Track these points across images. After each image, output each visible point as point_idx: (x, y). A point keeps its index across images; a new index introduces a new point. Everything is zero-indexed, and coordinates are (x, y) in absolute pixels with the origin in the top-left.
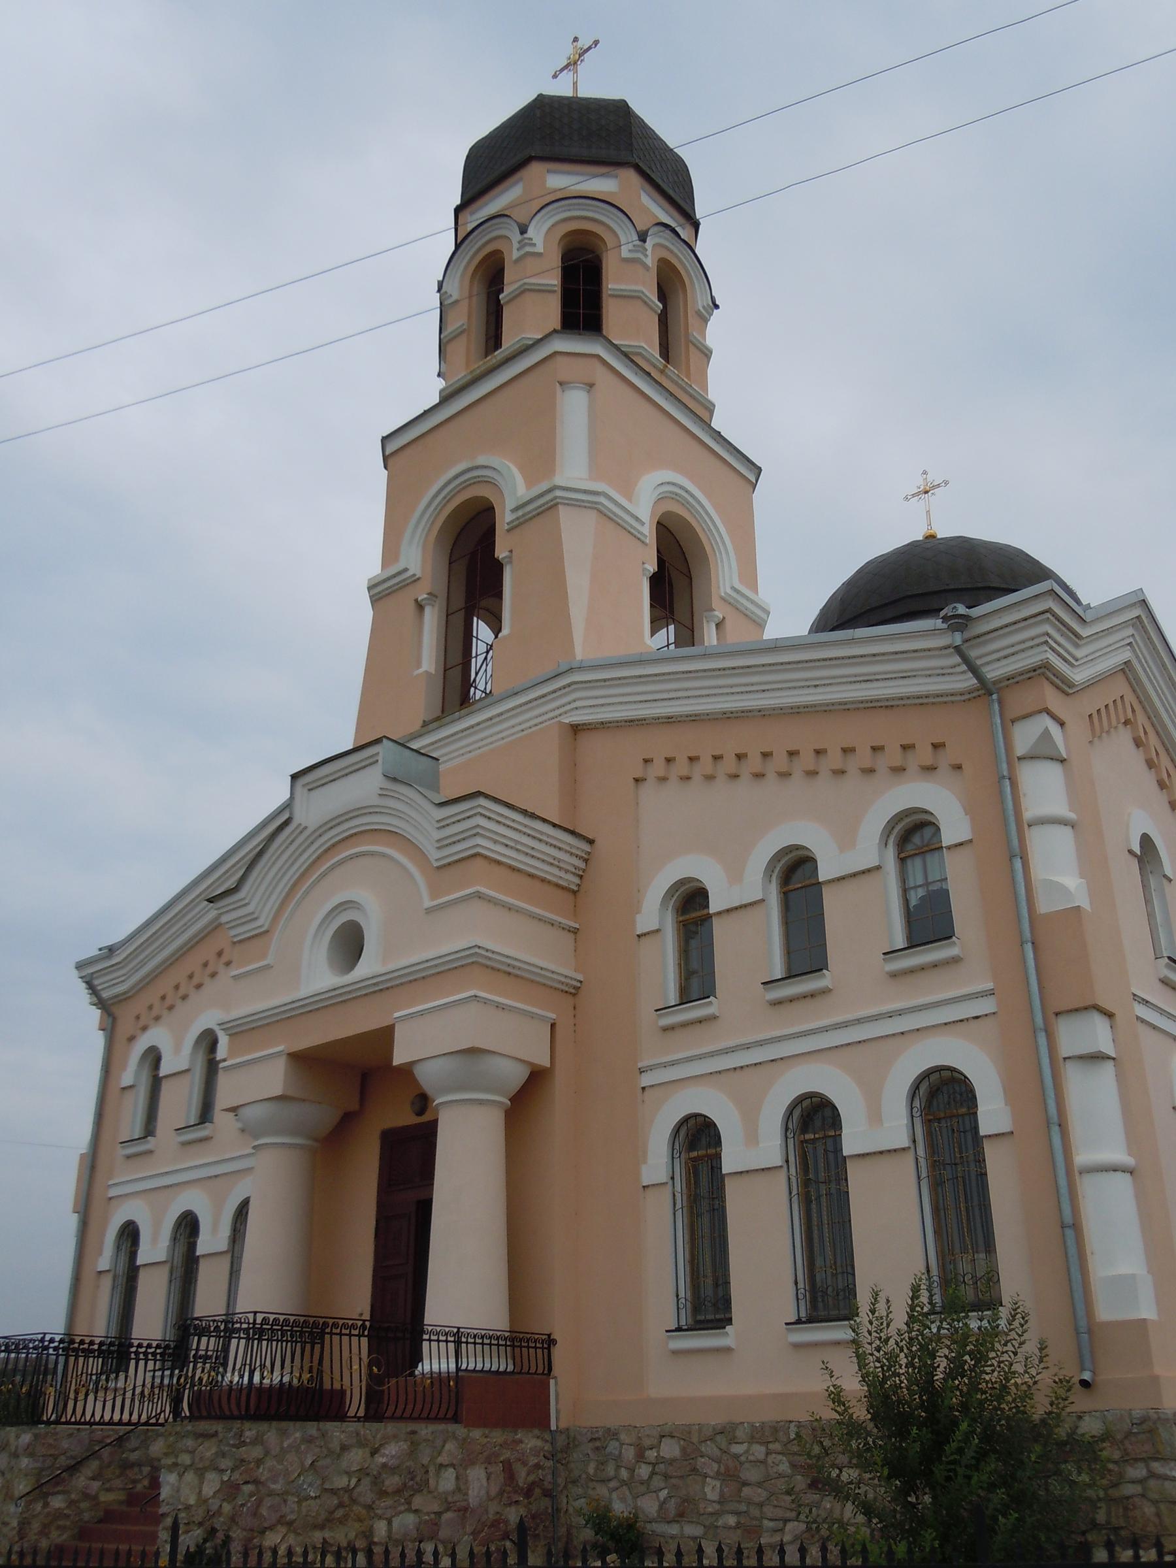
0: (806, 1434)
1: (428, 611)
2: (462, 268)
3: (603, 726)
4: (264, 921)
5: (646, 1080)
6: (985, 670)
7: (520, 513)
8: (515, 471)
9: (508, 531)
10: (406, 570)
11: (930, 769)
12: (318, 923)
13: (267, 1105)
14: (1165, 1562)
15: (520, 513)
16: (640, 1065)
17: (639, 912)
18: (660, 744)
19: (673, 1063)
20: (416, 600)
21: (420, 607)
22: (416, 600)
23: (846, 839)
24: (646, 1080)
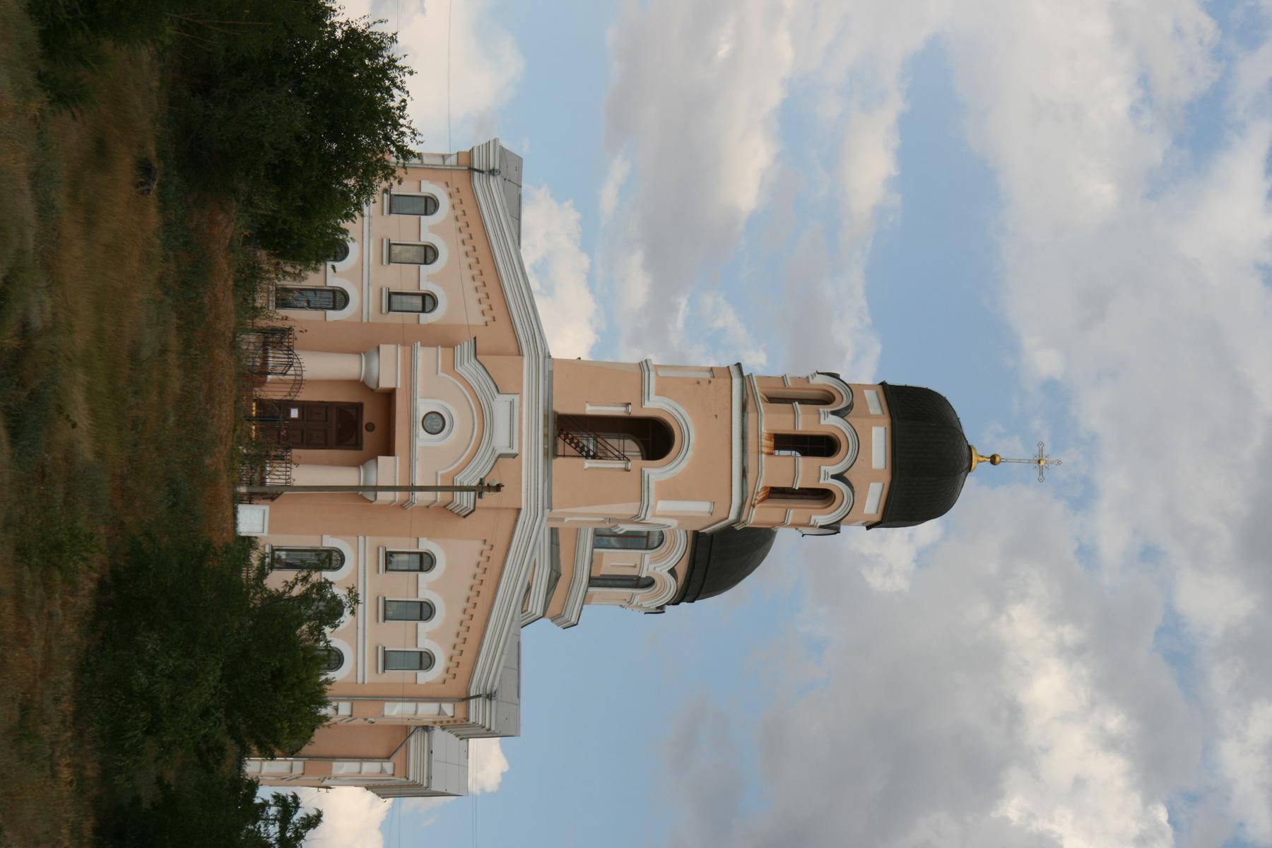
0: (264, 753)
1: (623, 409)
2: (839, 426)
3: (516, 521)
4: (459, 369)
5: (361, 538)
6: (474, 700)
7: (646, 479)
8: (684, 465)
9: (641, 470)
11: (447, 671)
12: (449, 409)
13: (377, 380)
14: (256, 804)
15: (646, 479)
16: (367, 538)
17: (428, 539)
18: (497, 556)
20: (630, 404)
21: (628, 404)
22: (630, 404)
23: (432, 636)
24: (361, 538)
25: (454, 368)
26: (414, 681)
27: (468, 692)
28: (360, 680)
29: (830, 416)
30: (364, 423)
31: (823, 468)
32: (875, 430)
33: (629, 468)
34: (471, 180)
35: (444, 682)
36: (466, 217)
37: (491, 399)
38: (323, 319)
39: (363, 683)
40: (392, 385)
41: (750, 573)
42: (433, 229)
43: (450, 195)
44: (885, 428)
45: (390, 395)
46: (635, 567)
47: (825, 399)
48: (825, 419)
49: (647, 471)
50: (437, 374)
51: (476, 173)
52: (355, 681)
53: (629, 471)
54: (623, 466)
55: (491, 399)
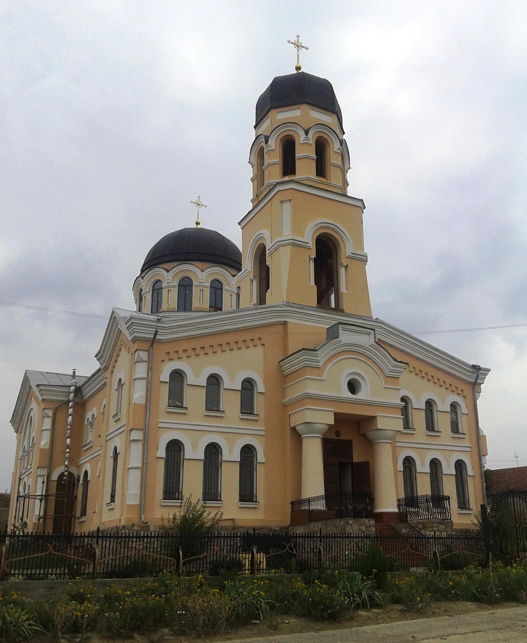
1: (311, 261)
7: (353, 255)
10: (308, 243)
15: (353, 255)
16: (397, 440)
19: (404, 442)
21: (310, 259)
25: (320, 368)
26: (466, 415)
27: (470, 383)
28: (469, 450)
29: (269, 143)
30: (335, 437)
31: (302, 142)
32: (311, 115)
33: (346, 265)
34: (160, 342)
35: (465, 397)
36: (214, 346)
37: (340, 344)
38: (263, 465)
39: (470, 447)
40: (332, 415)
41: (217, 232)
42: (197, 375)
43: (171, 360)
44: (278, 112)
45: (338, 416)
46: (231, 295)
47: (261, 154)
48: (309, 140)
49: (348, 253)
50: (324, 381)
51: (157, 337)
52: (469, 454)
53: (347, 265)
54: (343, 268)
55: (340, 344)
